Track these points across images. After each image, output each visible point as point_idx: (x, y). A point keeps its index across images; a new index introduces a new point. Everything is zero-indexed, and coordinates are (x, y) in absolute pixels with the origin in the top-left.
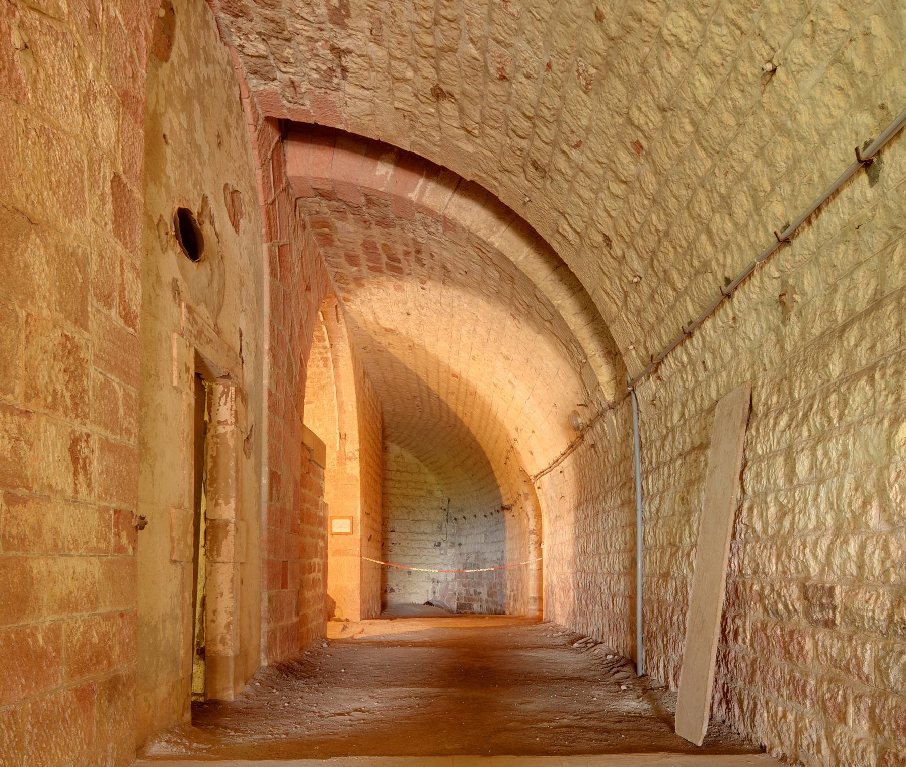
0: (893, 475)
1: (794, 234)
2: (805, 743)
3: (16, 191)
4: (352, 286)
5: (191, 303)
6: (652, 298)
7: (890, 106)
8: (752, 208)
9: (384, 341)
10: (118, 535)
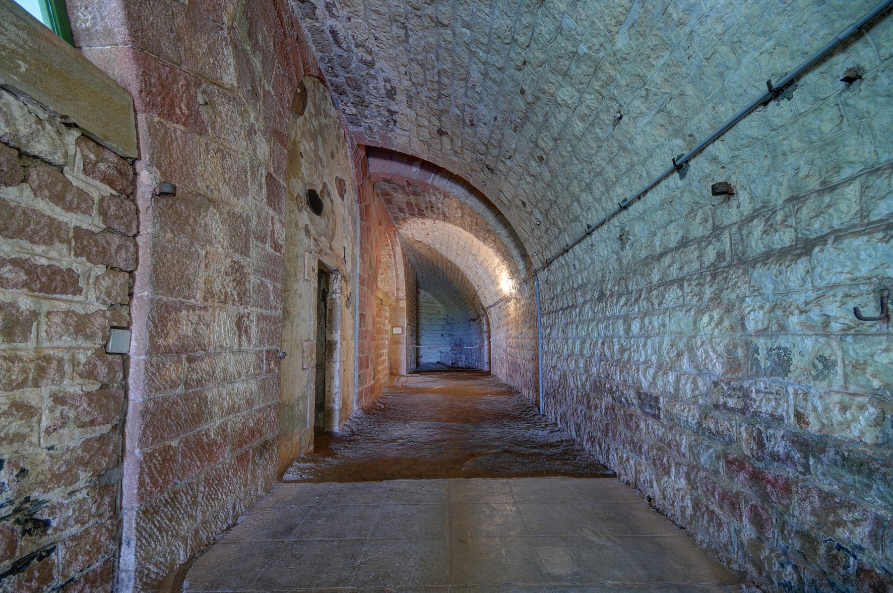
0: (699, 343)
1: (629, 204)
2: (642, 479)
3: (199, 184)
4: (402, 222)
5: (316, 236)
6: (546, 232)
7: (696, 135)
8: (604, 189)
9: (416, 246)
10: (269, 364)
